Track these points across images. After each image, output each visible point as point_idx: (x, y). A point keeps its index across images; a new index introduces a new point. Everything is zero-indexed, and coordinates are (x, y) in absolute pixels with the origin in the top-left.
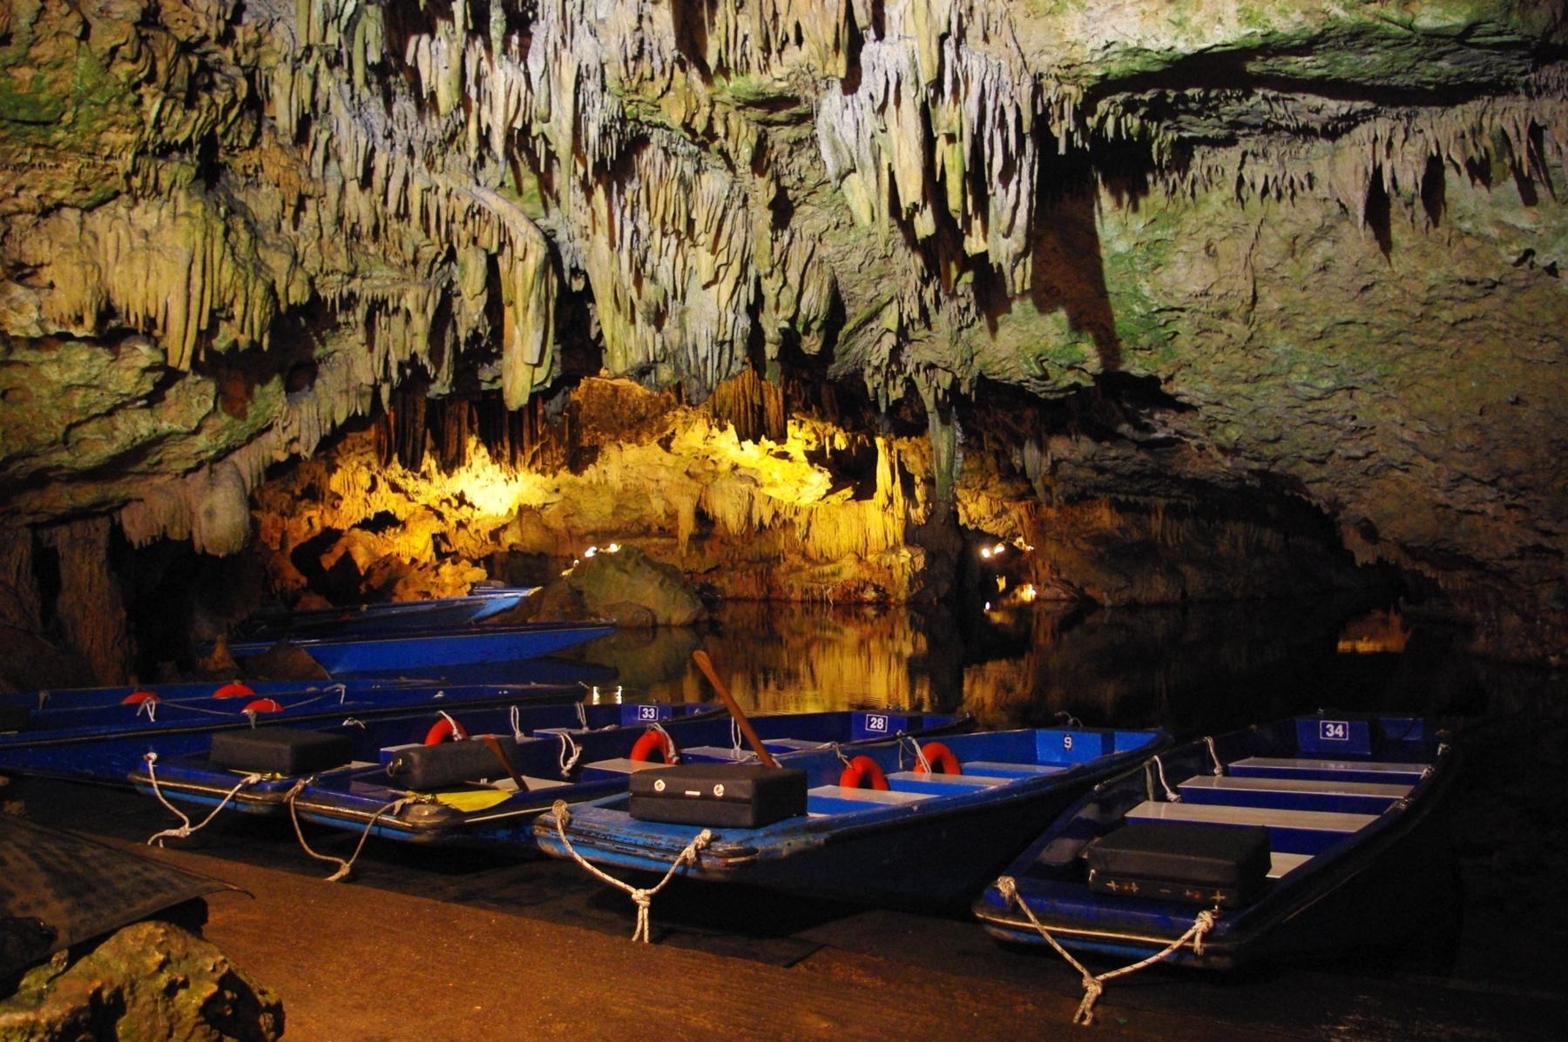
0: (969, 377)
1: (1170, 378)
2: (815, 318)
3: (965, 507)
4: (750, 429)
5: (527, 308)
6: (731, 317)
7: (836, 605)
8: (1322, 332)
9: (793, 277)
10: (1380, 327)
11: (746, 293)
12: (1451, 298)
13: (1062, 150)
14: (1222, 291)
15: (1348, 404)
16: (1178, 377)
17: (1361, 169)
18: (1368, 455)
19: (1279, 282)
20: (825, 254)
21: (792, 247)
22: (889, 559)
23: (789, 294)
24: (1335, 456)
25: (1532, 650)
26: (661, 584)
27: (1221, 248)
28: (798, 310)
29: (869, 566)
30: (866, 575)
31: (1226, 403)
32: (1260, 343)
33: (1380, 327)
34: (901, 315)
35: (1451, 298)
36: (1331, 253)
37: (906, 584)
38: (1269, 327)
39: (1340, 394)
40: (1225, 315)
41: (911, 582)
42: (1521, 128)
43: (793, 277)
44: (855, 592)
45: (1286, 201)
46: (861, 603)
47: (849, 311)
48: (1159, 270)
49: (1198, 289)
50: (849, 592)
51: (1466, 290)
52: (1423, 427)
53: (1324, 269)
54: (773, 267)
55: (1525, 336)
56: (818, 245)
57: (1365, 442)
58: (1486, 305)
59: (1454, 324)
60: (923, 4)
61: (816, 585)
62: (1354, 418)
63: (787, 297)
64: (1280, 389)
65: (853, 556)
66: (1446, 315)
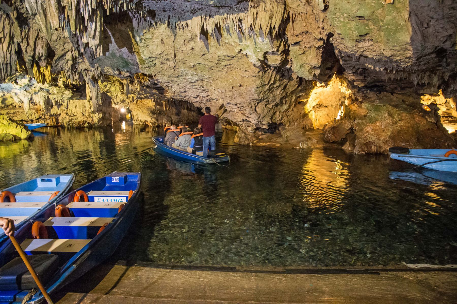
0: (97, 74)
1: (155, 75)
2: (42, 56)
3: (113, 100)
4: (41, 80)
6: (9, 55)
7: (77, 128)
8: (193, 66)
9: (32, 43)
10: (207, 65)
11: (14, 48)
12: (224, 59)
13: (108, 14)
14: (166, 53)
15: (201, 84)
16: (157, 75)
17: (199, 24)
18: (207, 96)
19: (181, 52)
20: (43, 35)
21: (29, 33)
23: (30, 48)
24: (200, 96)
25: (247, 142)
26: (17, 127)
27: (165, 41)
28: (35, 54)
30: (86, 119)
31: (171, 82)
32: (177, 68)
33: (207, 65)
34: (72, 55)
35: (224, 59)
36: (194, 45)
38: (179, 63)
39: (199, 81)
40: (168, 59)
42: (237, 19)
43: (32, 43)
45: (181, 30)
46: (84, 127)
47: (56, 53)
48: (149, 46)
49: (160, 52)
50: (81, 125)
51: (227, 58)
52: (219, 90)
53: (193, 49)
54: (22, 40)
55: (241, 70)
56: (40, 32)
57: (206, 93)
58: (232, 62)
59: (225, 66)
62: (203, 87)
63: (30, 49)
64: (184, 79)
65: (82, 114)
66: (223, 63)
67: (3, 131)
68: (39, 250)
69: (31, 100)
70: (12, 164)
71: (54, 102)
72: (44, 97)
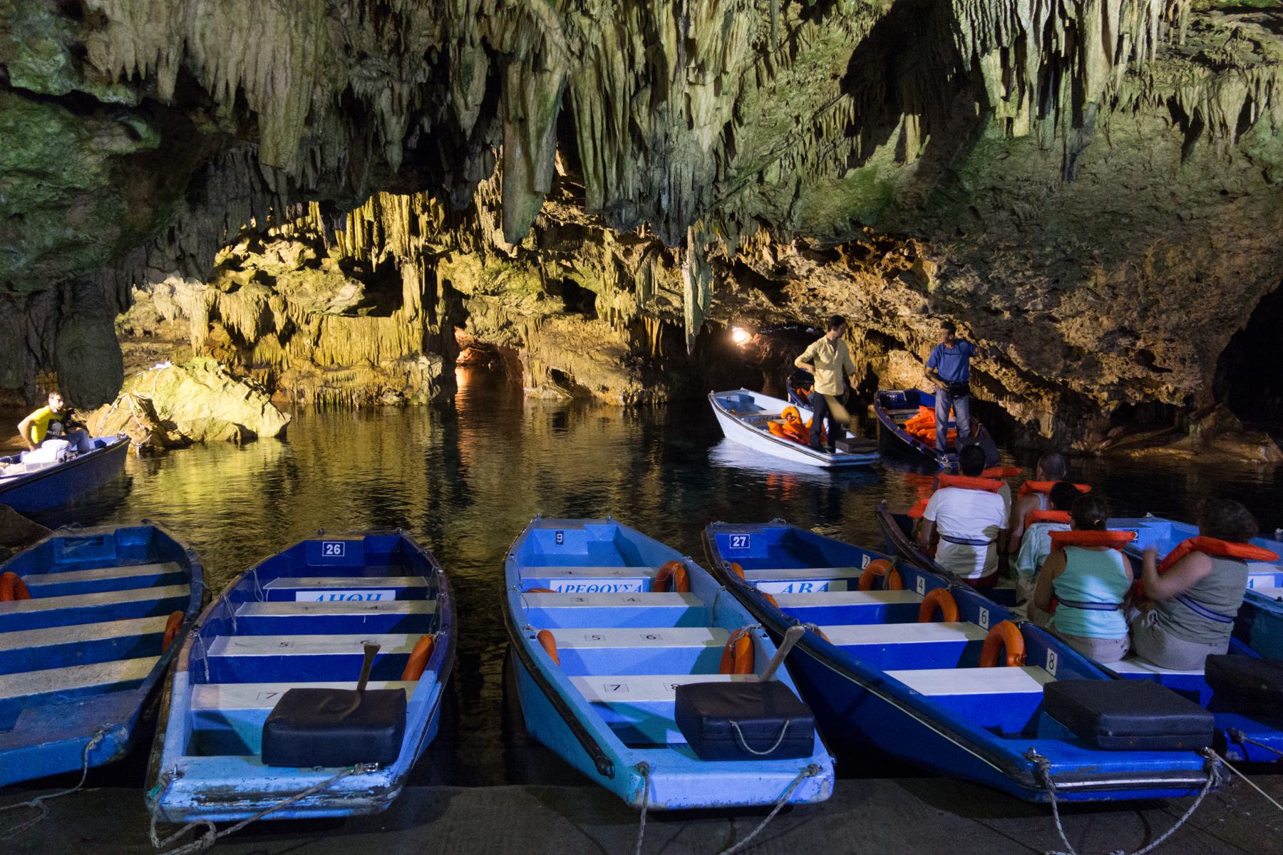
3: (472, 320)
5: (540, 133)
22: (410, 365)
26: (247, 398)
29: (383, 372)
30: (381, 379)
37: (426, 389)
41: (430, 388)
44: (377, 397)
60: (1049, 2)
61: (330, 390)
65: (367, 363)
67: (201, 409)
68: (639, 707)
69: (214, 314)
70: (617, 497)
71: (280, 321)
72: (257, 303)
